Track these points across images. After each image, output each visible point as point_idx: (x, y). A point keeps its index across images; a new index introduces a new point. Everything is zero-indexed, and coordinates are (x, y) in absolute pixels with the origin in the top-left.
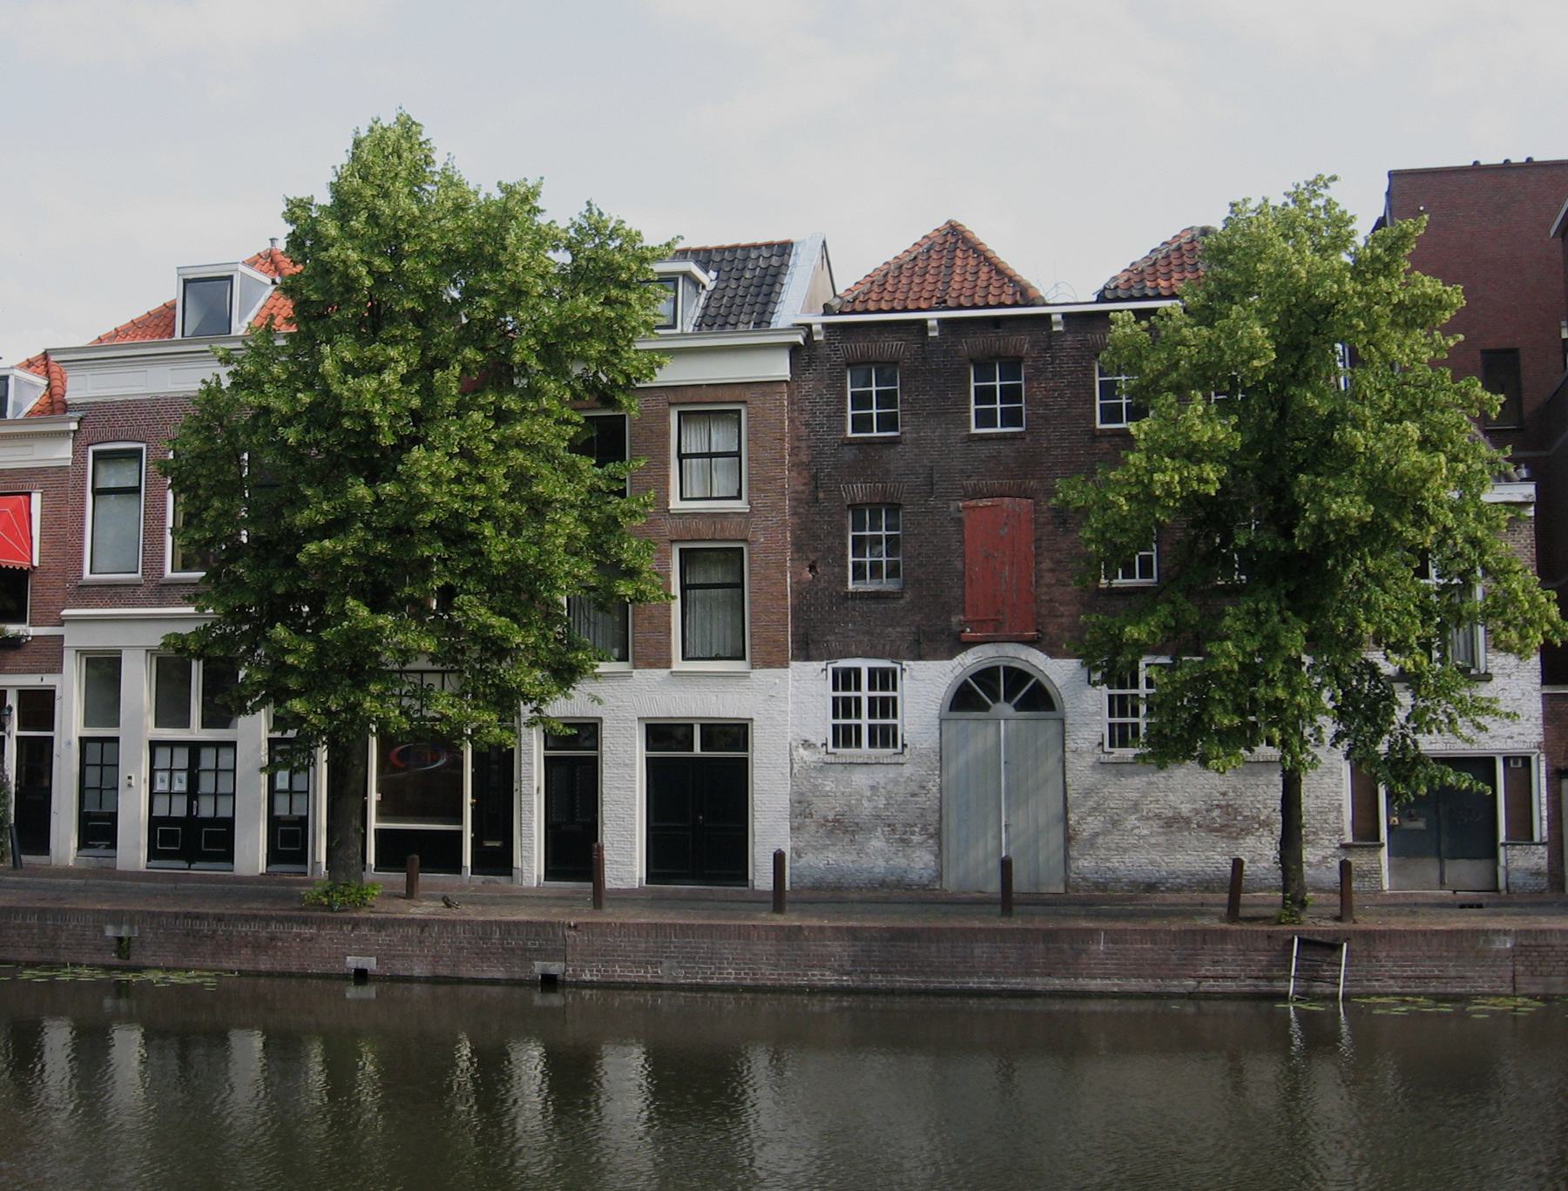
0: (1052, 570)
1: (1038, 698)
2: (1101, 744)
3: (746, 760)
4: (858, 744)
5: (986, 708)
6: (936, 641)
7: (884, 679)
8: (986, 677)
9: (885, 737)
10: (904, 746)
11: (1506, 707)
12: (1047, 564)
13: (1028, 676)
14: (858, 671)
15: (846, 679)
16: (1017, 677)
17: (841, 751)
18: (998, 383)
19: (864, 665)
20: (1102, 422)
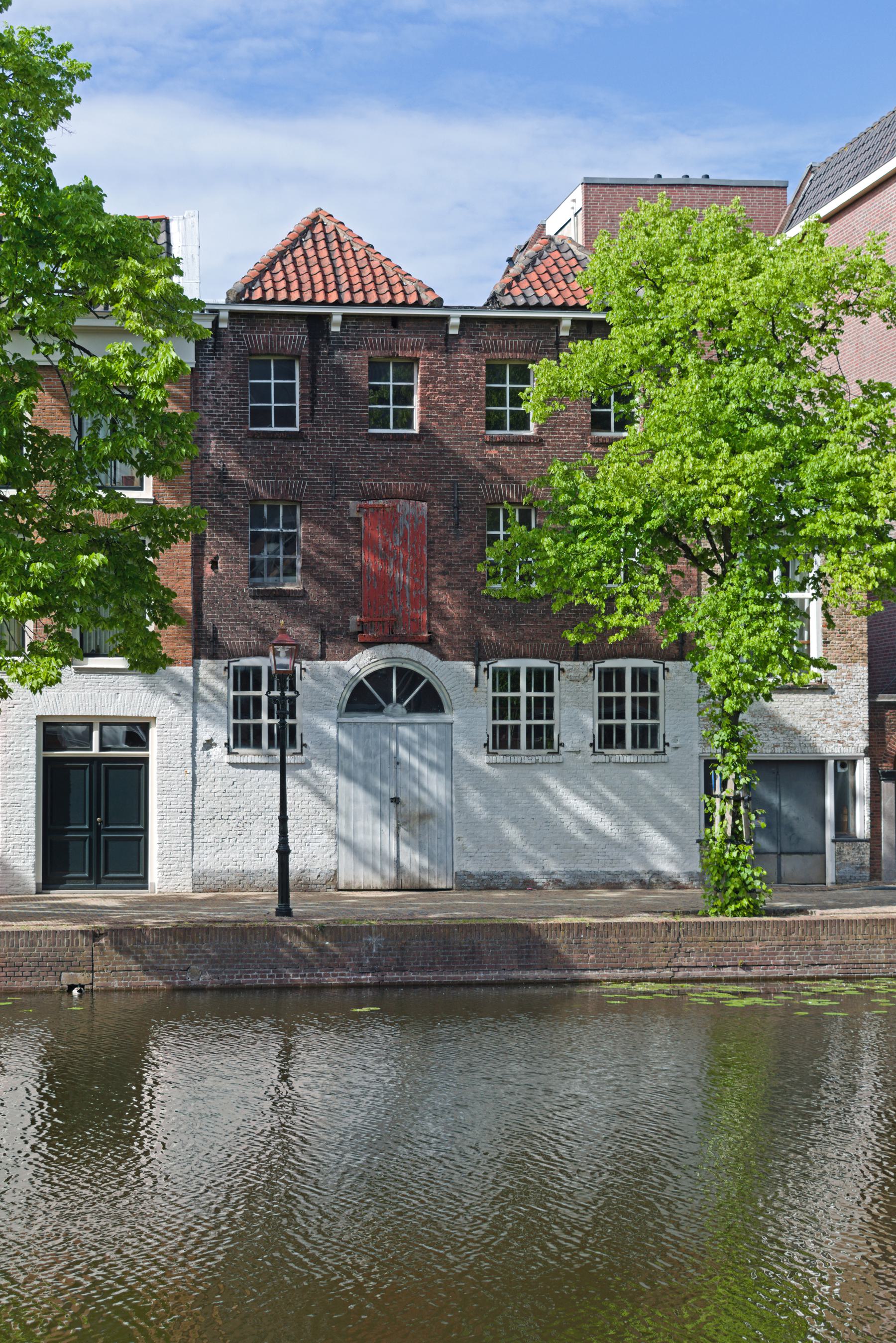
0: (443, 573)
1: (429, 701)
2: (486, 745)
3: (45, 749)
4: (516, 745)
5: (379, 710)
6: (335, 637)
7: (541, 679)
8: (380, 678)
9: (646, 738)
10: (561, 745)
11: (831, 719)
12: (439, 567)
13: (418, 678)
14: (621, 672)
15: (506, 679)
16: (409, 679)
17: (607, 751)
18: (391, 384)
19: (523, 664)
20: (294, 425)
